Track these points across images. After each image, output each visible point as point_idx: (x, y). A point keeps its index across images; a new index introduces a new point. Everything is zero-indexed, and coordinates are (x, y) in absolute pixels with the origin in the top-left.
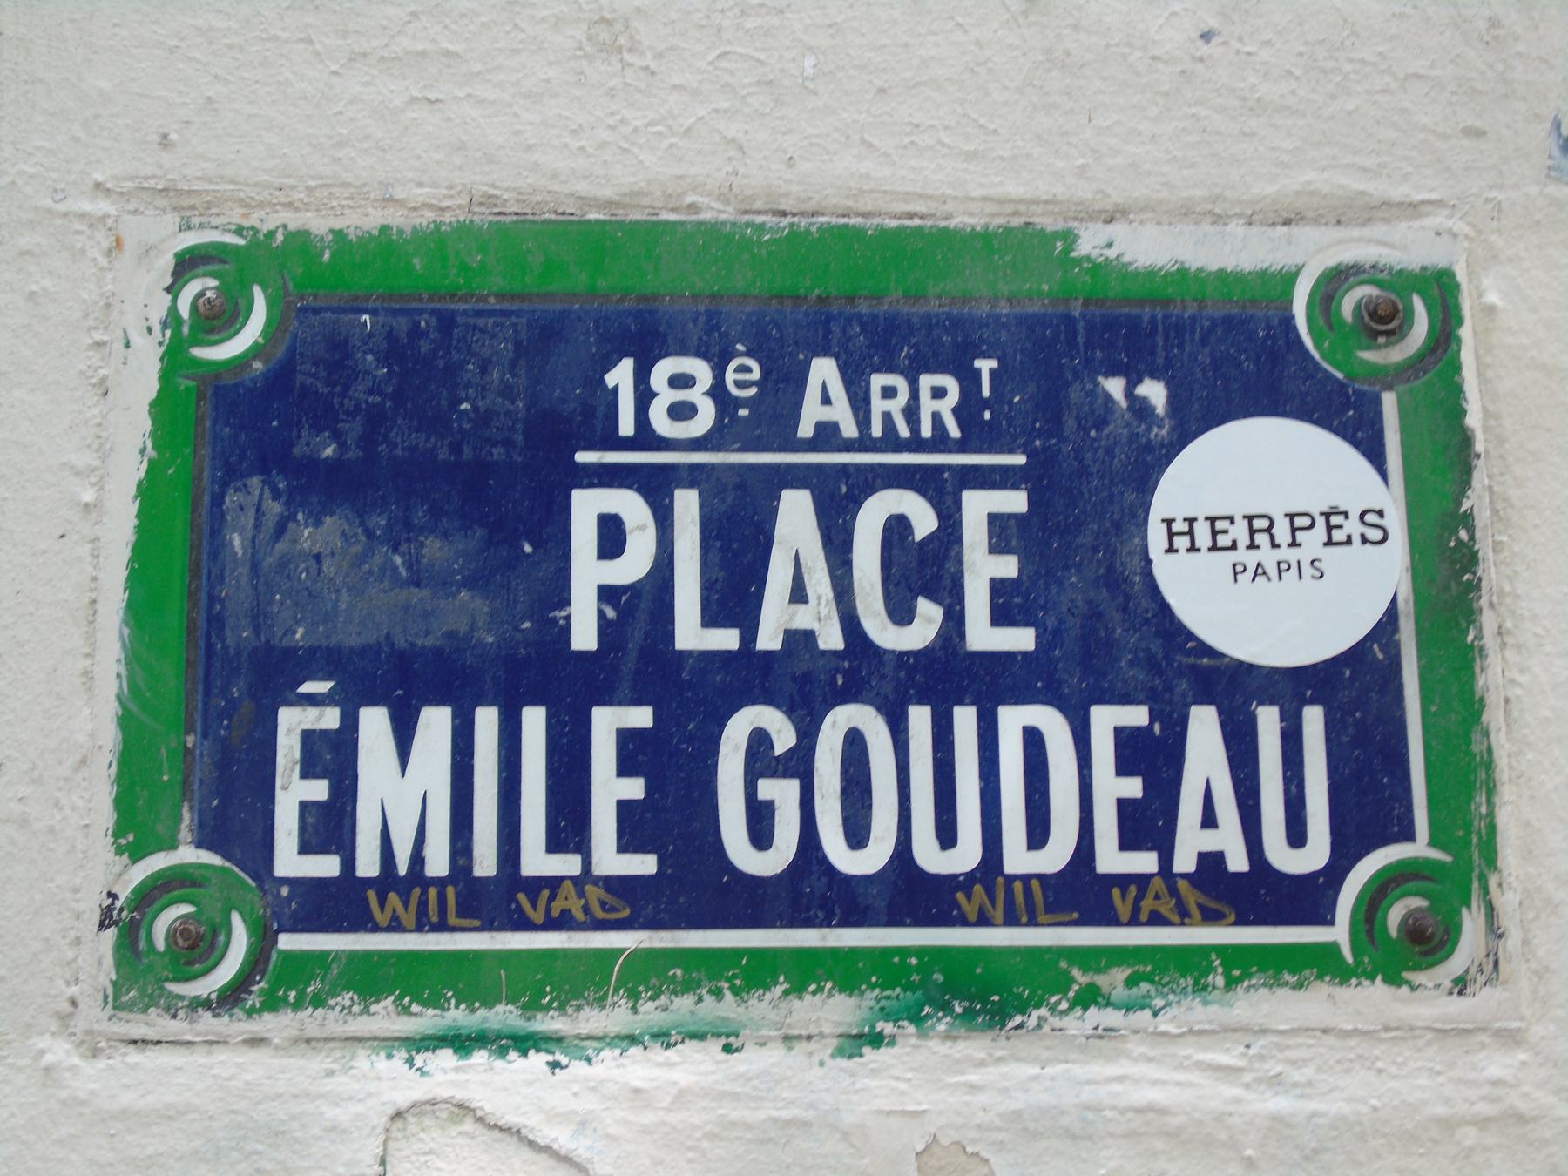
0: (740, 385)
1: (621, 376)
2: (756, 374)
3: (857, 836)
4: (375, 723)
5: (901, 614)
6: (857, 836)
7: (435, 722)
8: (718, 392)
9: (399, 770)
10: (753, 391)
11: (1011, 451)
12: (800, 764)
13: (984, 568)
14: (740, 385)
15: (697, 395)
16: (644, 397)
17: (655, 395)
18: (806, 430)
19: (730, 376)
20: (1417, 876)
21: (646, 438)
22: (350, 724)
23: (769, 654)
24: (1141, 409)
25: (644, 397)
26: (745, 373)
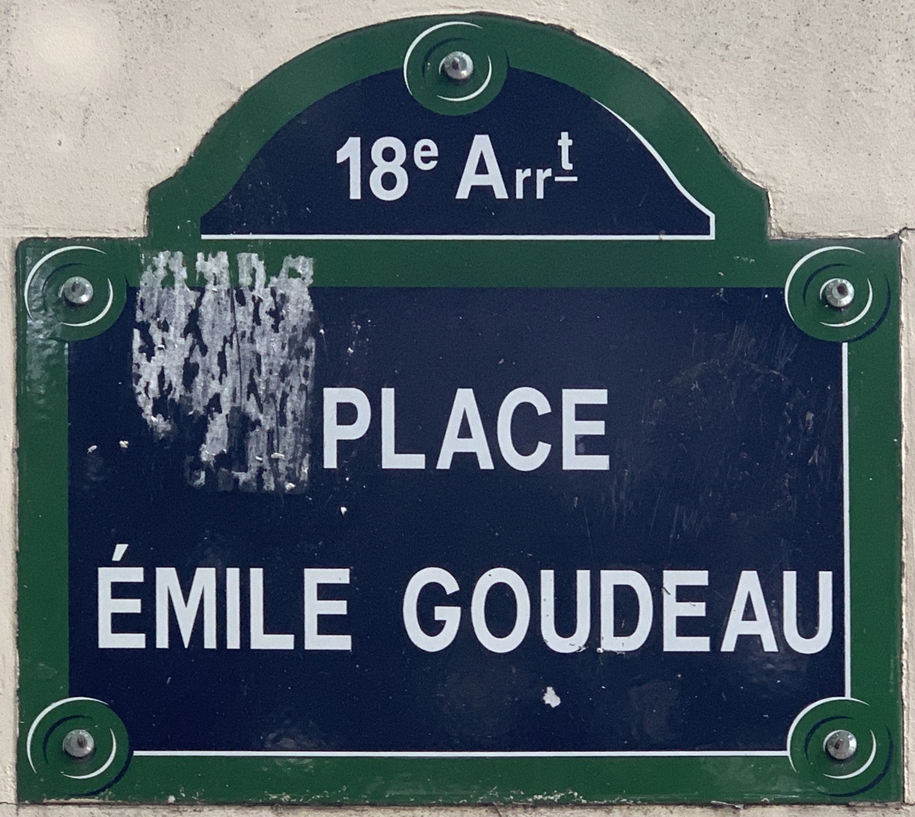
0: (426, 160)
1: (350, 151)
2: (434, 152)
3: (566, 627)
4: (167, 577)
7: (205, 577)
8: (409, 165)
9: (467, 413)
10: (433, 164)
12: (463, 600)
13: (573, 428)
14: (426, 160)
15: (396, 167)
16: (367, 166)
18: (304, 266)
19: (418, 154)
21: (234, 250)
22: (150, 578)
24: (357, 328)
25: (367, 166)
26: (427, 151)
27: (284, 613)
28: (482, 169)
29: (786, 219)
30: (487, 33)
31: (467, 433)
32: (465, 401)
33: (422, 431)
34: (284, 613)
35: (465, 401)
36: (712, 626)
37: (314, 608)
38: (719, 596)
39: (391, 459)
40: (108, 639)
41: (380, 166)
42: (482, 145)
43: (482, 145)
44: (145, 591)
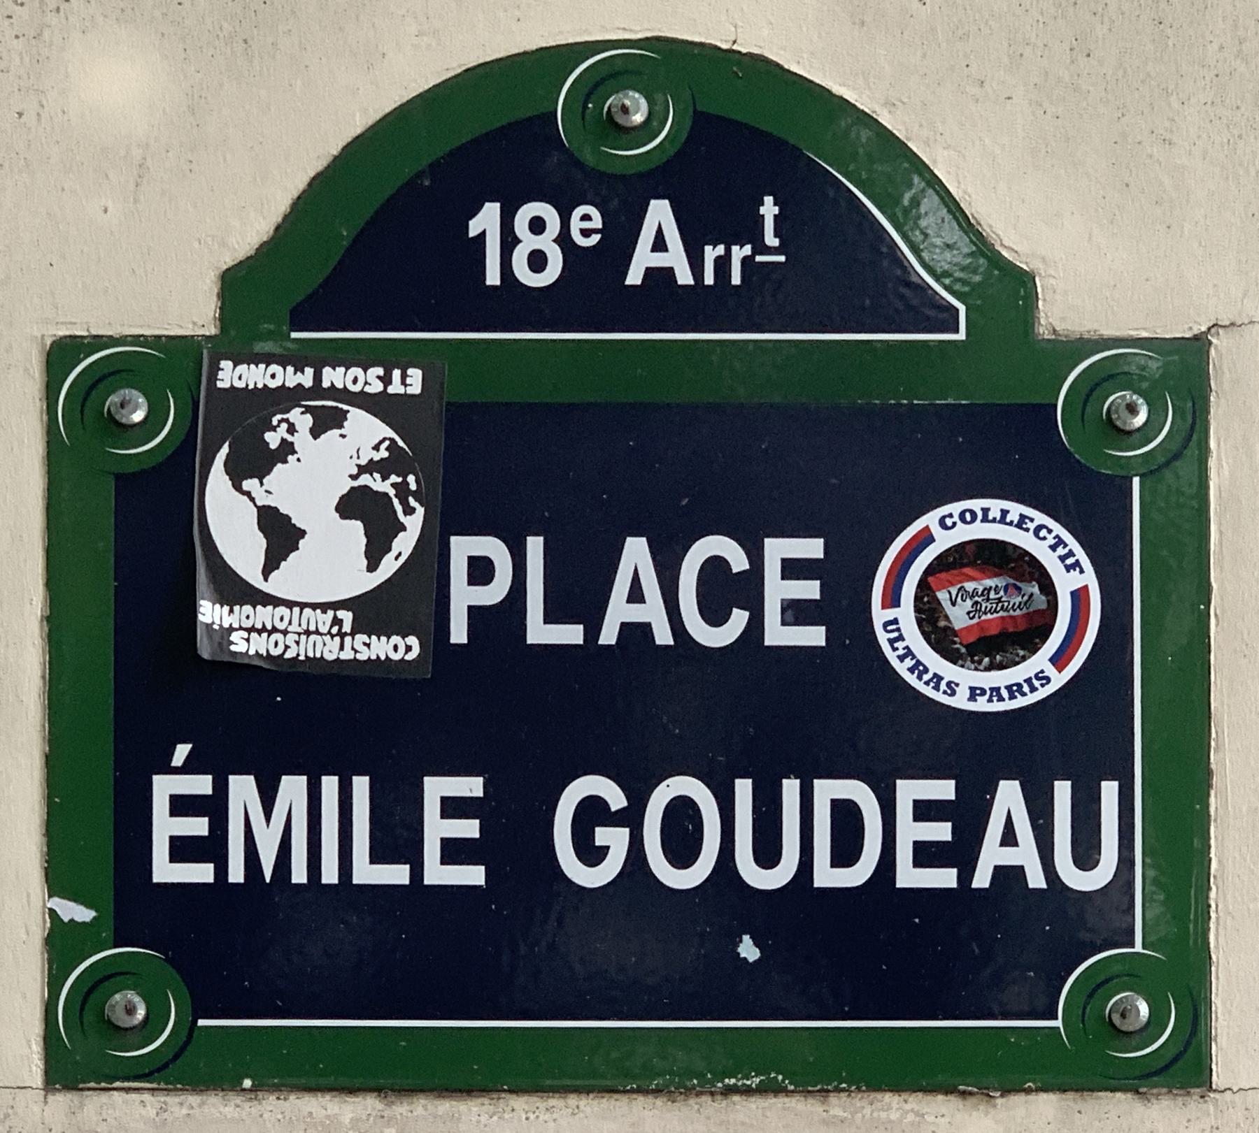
0: (586, 233)
1: (486, 220)
3: (767, 855)
4: (242, 789)
5: (715, 617)
6: (767, 855)
7: (293, 788)
8: (564, 239)
10: (596, 238)
11: (206, 1027)
13: (778, 590)
14: (586, 233)
16: (509, 241)
17: (519, 241)
19: (576, 225)
20: (614, 75)
22: (221, 789)
23: (608, 647)
25: (509, 241)
26: (587, 221)
27: (397, 836)
28: (660, 244)
29: (1059, 313)
30: (665, 62)
31: (640, 596)
32: (636, 553)
33: (578, 594)
34: (397, 836)
35: (636, 553)
36: (961, 852)
37: (437, 829)
38: (969, 816)
39: (539, 632)
40: (164, 871)
41: (526, 242)
42: (660, 213)
43: (660, 213)
44: (214, 807)
